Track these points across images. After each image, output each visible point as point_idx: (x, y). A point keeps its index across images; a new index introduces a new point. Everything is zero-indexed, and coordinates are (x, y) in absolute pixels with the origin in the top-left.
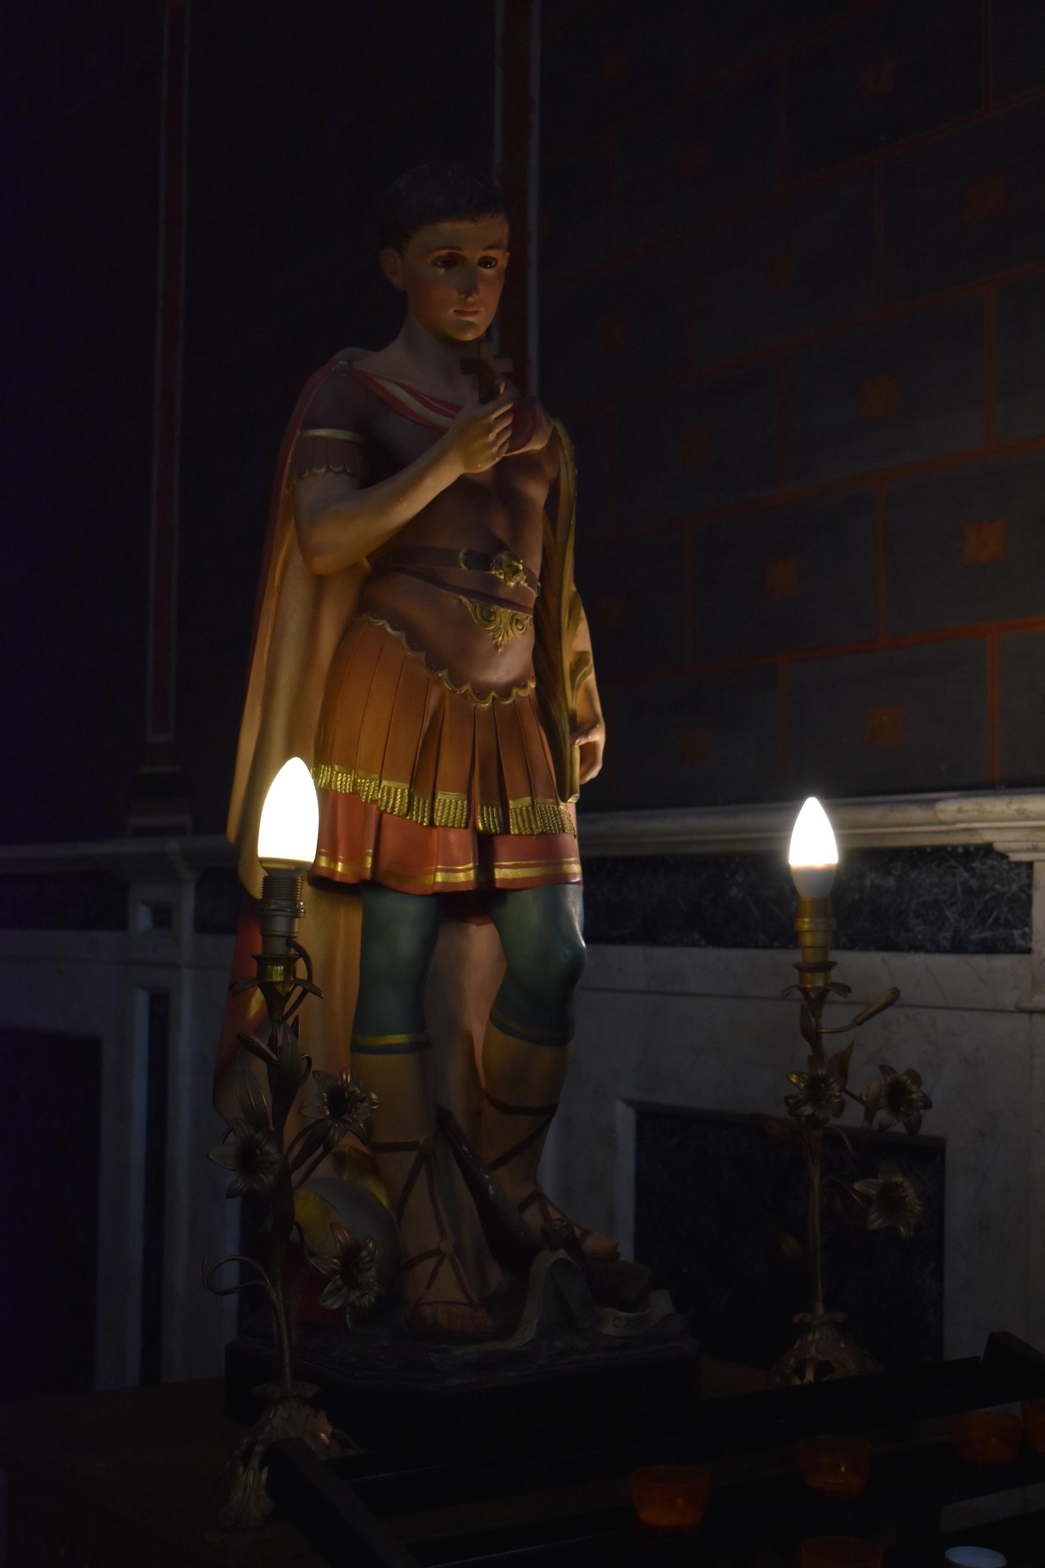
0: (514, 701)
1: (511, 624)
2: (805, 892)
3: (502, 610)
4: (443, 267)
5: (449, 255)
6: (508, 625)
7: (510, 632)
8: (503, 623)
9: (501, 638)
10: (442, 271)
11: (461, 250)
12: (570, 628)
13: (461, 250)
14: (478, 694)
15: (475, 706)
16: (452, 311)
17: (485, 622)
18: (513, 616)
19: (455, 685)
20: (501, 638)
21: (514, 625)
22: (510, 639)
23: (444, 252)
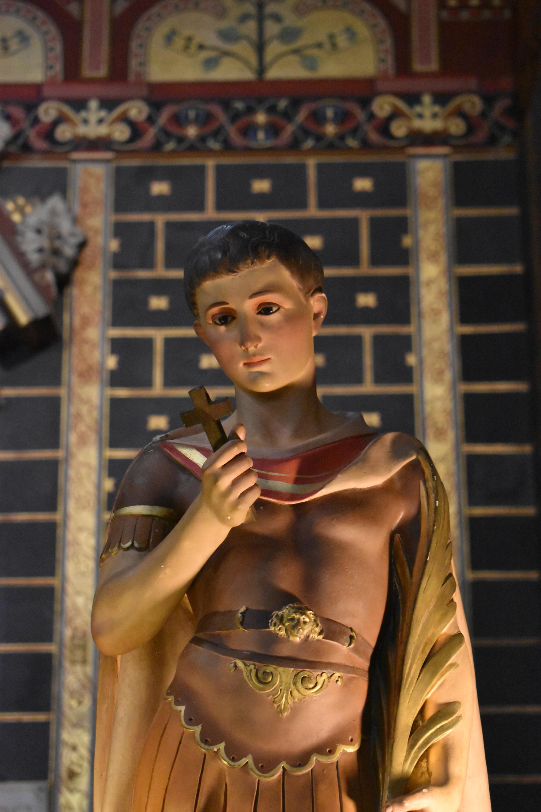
0: (312, 770)
1: (295, 684)
2: (305, 612)
3: (281, 669)
4: (222, 324)
5: (221, 312)
6: (292, 686)
7: (295, 693)
8: (283, 684)
9: (284, 700)
10: (223, 328)
11: (227, 303)
12: (418, 682)
13: (227, 303)
14: (262, 766)
15: (259, 780)
16: (241, 365)
17: (261, 686)
18: (296, 675)
19: (233, 760)
20: (284, 700)
21: (299, 684)
22: (296, 700)
23: (215, 310)
